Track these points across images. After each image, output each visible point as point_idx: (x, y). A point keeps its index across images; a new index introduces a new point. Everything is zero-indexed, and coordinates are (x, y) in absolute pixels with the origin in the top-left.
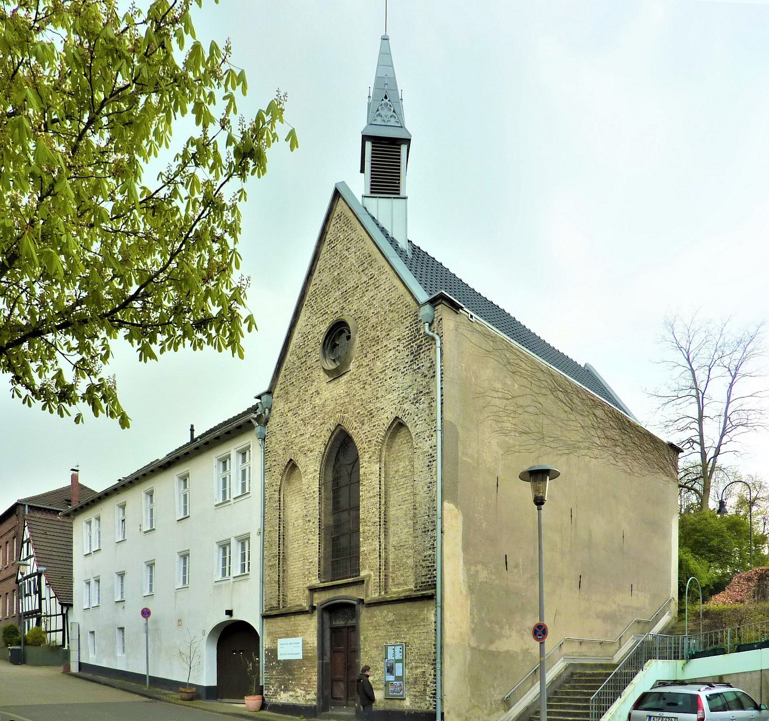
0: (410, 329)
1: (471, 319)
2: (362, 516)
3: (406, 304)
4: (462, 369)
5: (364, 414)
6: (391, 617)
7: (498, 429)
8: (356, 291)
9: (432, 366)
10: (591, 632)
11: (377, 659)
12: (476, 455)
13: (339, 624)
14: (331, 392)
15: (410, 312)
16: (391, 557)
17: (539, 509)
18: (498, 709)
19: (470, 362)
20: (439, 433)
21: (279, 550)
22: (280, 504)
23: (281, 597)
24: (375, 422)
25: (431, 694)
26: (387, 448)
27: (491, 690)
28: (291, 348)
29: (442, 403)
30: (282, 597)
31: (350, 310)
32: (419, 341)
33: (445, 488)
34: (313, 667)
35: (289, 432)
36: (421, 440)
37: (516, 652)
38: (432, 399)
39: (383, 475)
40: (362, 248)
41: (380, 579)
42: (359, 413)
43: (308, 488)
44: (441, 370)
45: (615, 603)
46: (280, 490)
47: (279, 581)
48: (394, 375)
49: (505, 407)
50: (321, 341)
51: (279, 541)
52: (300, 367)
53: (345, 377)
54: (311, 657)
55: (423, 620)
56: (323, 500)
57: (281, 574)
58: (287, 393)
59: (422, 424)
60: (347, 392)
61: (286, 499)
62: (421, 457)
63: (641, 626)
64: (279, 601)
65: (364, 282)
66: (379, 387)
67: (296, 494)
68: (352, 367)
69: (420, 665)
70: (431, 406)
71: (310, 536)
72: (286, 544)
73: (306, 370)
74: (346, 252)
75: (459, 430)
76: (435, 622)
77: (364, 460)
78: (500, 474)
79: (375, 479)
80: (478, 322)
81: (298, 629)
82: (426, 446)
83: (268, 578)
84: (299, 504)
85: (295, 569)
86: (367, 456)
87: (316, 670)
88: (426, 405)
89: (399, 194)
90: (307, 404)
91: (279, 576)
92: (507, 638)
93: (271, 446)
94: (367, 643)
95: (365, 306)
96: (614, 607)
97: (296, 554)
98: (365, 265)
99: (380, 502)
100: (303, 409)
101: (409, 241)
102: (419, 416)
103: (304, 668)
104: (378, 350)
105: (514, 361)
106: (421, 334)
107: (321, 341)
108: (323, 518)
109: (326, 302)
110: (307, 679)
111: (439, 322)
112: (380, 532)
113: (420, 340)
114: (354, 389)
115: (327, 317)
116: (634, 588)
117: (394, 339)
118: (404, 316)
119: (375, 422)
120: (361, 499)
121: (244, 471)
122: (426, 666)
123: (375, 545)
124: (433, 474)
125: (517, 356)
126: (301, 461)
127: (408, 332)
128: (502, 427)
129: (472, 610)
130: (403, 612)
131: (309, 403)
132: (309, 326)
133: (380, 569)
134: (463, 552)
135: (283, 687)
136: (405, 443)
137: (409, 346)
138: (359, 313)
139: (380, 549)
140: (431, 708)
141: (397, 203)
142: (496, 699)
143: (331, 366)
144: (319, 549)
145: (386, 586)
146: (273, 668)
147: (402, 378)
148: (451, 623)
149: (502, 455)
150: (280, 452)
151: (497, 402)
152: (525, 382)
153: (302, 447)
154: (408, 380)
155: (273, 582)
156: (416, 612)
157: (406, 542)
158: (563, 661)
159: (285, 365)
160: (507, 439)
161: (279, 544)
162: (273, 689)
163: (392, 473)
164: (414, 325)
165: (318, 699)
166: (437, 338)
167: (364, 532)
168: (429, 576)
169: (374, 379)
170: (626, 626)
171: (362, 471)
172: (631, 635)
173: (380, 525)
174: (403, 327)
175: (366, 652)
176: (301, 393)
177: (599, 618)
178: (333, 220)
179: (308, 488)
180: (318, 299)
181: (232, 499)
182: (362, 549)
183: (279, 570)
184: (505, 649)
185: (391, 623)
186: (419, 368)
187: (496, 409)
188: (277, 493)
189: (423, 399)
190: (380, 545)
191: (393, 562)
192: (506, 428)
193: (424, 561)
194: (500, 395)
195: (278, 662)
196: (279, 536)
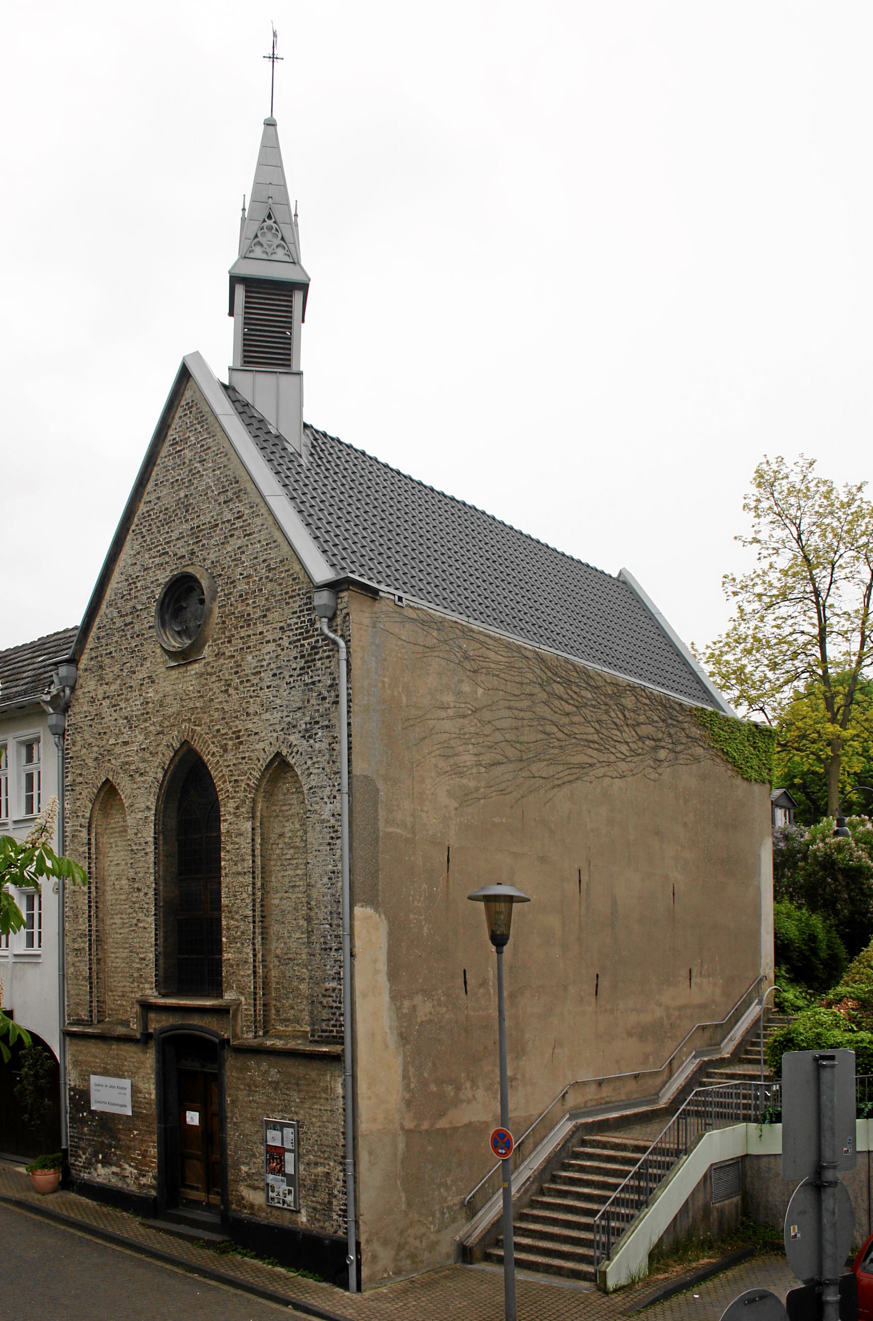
0: (299, 617)
1: (400, 604)
2: (224, 901)
3: (292, 574)
4: (384, 686)
5: (226, 734)
6: (274, 1074)
7: (449, 768)
8: (215, 531)
9: (334, 686)
10: (617, 1062)
11: (254, 1138)
12: (409, 820)
13: (191, 1065)
14: (175, 685)
15: (299, 589)
16: (274, 973)
17: (499, 952)
18: (454, 1220)
19: (398, 673)
20: (346, 797)
21: (90, 926)
22: (89, 849)
23: (95, 1004)
24: (243, 752)
25: (340, 1210)
26: (264, 797)
27: (442, 1190)
28: (109, 595)
29: (350, 748)
30: (99, 1011)
31: (204, 560)
32: (313, 640)
33: (357, 884)
34: (150, 1133)
35: (105, 733)
36: (317, 799)
37: (485, 1122)
38: (334, 738)
39: (258, 840)
40: (225, 466)
41: (255, 1011)
42: (218, 731)
43: (136, 834)
44: (349, 694)
45: (660, 1005)
46: (89, 826)
47: (90, 977)
48: (274, 684)
49: (460, 730)
50: (157, 597)
51: (90, 912)
52: (123, 630)
53: (197, 666)
54: (147, 1115)
55: (325, 1090)
56: (161, 858)
57: (94, 967)
58: (101, 667)
59: (318, 774)
60: (199, 692)
61: (101, 840)
62: (318, 827)
63: (707, 1034)
64: (91, 1011)
65: (228, 521)
66: (251, 697)
67: (118, 835)
68: (206, 651)
69: (322, 1161)
70: (333, 750)
71: (141, 916)
72: (101, 915)
73: (132, 637)
74: (198, 465)
75: (379, 786)
76: (343, 1097)
77: (227, 808)
78: (453, 841)
79: (245, 844)
80: (412, 604)
81: (123, 1065)
82: (326, 811)
83: (72, 969)
84: (122, 853)
85: (117, 960)
86: (232, 804)
87: (155, 1138)
88: (324, 746)
89: (289, 366)
90: (134, 694)
91: (90, 969)
92: (469, 1102)
93: (74, 749)
94: (236, 1110)
95: (228, 559)
96: (659, 1012)
97: (119, 936)
98: (230, 494)
99: (254, 884)
100: (128, 700)
101: (306, 426)
102: (315, 760)
103: (135, 1132)
104: (249, 636)
105: (476, 653)
106: (317, 630)
107: (157, 597)
108: (161, 888)
109: (166, 535)
110: (140, 1150)
111: (345, 617)
112: (254, 933)
113: (316, 638)
114: (211, 689)
115: (167, 560)
116: (693, 974)
117: (274, 626)
118: (290, 594)
119: (243, 752)
120: (223, 872)
121: (30, 777)
122: (332, 1164)
123: (247, 954)
124: (337, 857)
125: (481, 643)
126: (124, 786)
127: (295, 620)
128: (456, 764)
129: (405, 1070)
130: (293, 1070)
131: (137, 693)
132: (138, 567)
133: (255, 994)
134: (389, 980)
135: (100, 1157)
136: (293, 793)
137: (298, 644)
138: (219, 568)
139: (254, 961)
140: (340, 1233)
141: (286, 381)
142: (451, 1203)
143: (175, 644)
144: (156, 940)
145: (266, 1022)
146: (83, 1121)
147: (288, 691)
148: (370, 1098)
149: (456, 809)
150: (91, 763)
151: (447, 725)
152: (495, 681)
153: (127, 763)
154: (297, 698)
155: (81, 977)
156: (314, 1074)
157: (297, 954)
158: (569, 1119)
159: (98, 620)
160: (465, 781)
161: (90, 916)
162: (84, 1157)
163: (273, 836)
164: (306, 613)
165: (159, 1187)
166: (342, 643)
167: (229, 929)
168: (333, 1022)
169: (242, 682)
170: (680, 1040)
171: (224, 827)
172: (691, 1052)
173: (254, 922)
174: (288, 611)
175: (235, 1124)
176: (125, 674)
177: (632, 1036)
178: (180, 410)
179: (136, 834)
180: (154, 526)
181: (10, 823)
182: (226, 956)
183: (90, 959)
184: (466, 1121)
185: (275, 1085)
186: (313, 683)
187: (445, 736)
188: (85, 830)
189: (320, 734)
190: (255, 955)
191: (278, 983)
192: (461, 765)
193: (324, 996)
194: (451, 712)
195: (93, 1113)
196: (90, 902)
